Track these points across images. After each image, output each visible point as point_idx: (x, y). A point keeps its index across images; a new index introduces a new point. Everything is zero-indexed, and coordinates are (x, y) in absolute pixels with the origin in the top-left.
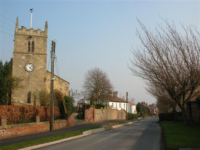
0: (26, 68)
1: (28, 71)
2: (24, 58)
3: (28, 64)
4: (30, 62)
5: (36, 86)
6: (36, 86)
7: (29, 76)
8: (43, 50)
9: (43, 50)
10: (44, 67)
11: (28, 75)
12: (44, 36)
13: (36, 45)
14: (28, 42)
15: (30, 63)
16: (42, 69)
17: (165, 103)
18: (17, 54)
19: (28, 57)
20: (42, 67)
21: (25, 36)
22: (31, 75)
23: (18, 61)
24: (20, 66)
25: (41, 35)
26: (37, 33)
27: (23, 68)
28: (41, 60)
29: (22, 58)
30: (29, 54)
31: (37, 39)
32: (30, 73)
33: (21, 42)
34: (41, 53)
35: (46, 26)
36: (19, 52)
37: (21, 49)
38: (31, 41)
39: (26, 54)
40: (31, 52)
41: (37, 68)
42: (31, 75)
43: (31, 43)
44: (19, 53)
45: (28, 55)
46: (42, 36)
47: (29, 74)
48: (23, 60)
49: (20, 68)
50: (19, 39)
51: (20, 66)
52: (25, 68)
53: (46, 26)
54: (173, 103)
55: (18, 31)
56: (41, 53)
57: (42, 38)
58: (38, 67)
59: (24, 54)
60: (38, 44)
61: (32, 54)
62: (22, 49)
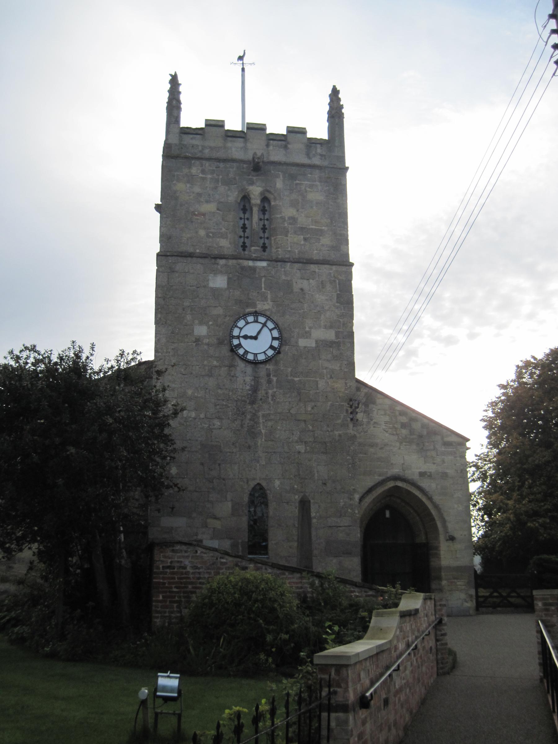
0: (270, 353)
1: (250, 357)
2: (219, 282)
3: (244, 316)
4: (260, 306)
5: (301, 448)
6: (301, 448)
7: (255, 389)
8: (326, 241)
9: (326, 241)
10: (337, 334)
11: (248, 379)
12: (326, 163)
13: (285, 210)
14: (233, 196)
15: (256, 314)
16: (330, 344)
17: (329, 410)
18: (181, 265)
19: (242, 277)
20: (331, 335)
21: (222, 165)
22: (263, 381)
23: (187, 303)
24: (201, 330)
25: (308, 155)
26: (286, 147)
27: (221, 342)
28: (320, 298)
29: (211, 285)
30: (251, 263)
31: (293, 177)
32: (262, 371)
33: (199, 195)
34: (315, 255)
35: (336, 115)
36: (191, 250)
37: (202, 233)
38: (256, 191)
39: (231, 262)
40: (254, 250)
41: (302, 343)
42: (263, 381)
43: (256, 200)
44: (191, 255)
45: (243, 268)
46: (316, 161)
47: (256, 379)
48: (216, 293)
49: (198, 340)
50: (191, 179)
51: (201, 330)
52: (231, 343)
53: (336, 115)
54: (357, 405)
55: (181, 140)
56: (315, 257)
57: (317, 174)
58: (307, 335)
59: (222, 262)
60: (294, 204)
61: (264, 264)
62: (208, 236)
